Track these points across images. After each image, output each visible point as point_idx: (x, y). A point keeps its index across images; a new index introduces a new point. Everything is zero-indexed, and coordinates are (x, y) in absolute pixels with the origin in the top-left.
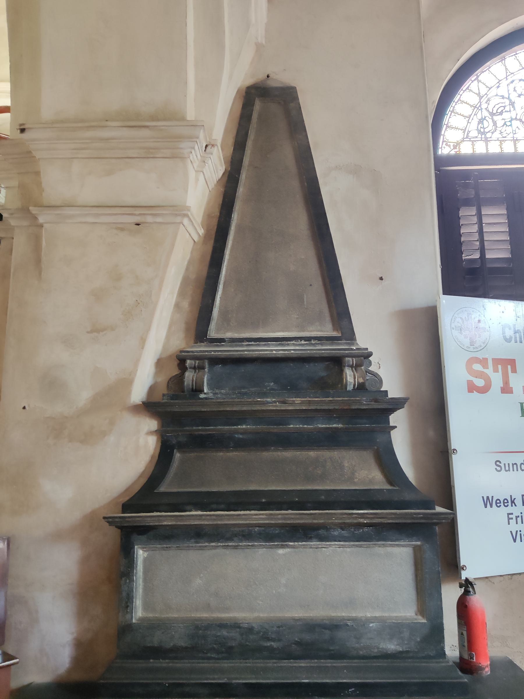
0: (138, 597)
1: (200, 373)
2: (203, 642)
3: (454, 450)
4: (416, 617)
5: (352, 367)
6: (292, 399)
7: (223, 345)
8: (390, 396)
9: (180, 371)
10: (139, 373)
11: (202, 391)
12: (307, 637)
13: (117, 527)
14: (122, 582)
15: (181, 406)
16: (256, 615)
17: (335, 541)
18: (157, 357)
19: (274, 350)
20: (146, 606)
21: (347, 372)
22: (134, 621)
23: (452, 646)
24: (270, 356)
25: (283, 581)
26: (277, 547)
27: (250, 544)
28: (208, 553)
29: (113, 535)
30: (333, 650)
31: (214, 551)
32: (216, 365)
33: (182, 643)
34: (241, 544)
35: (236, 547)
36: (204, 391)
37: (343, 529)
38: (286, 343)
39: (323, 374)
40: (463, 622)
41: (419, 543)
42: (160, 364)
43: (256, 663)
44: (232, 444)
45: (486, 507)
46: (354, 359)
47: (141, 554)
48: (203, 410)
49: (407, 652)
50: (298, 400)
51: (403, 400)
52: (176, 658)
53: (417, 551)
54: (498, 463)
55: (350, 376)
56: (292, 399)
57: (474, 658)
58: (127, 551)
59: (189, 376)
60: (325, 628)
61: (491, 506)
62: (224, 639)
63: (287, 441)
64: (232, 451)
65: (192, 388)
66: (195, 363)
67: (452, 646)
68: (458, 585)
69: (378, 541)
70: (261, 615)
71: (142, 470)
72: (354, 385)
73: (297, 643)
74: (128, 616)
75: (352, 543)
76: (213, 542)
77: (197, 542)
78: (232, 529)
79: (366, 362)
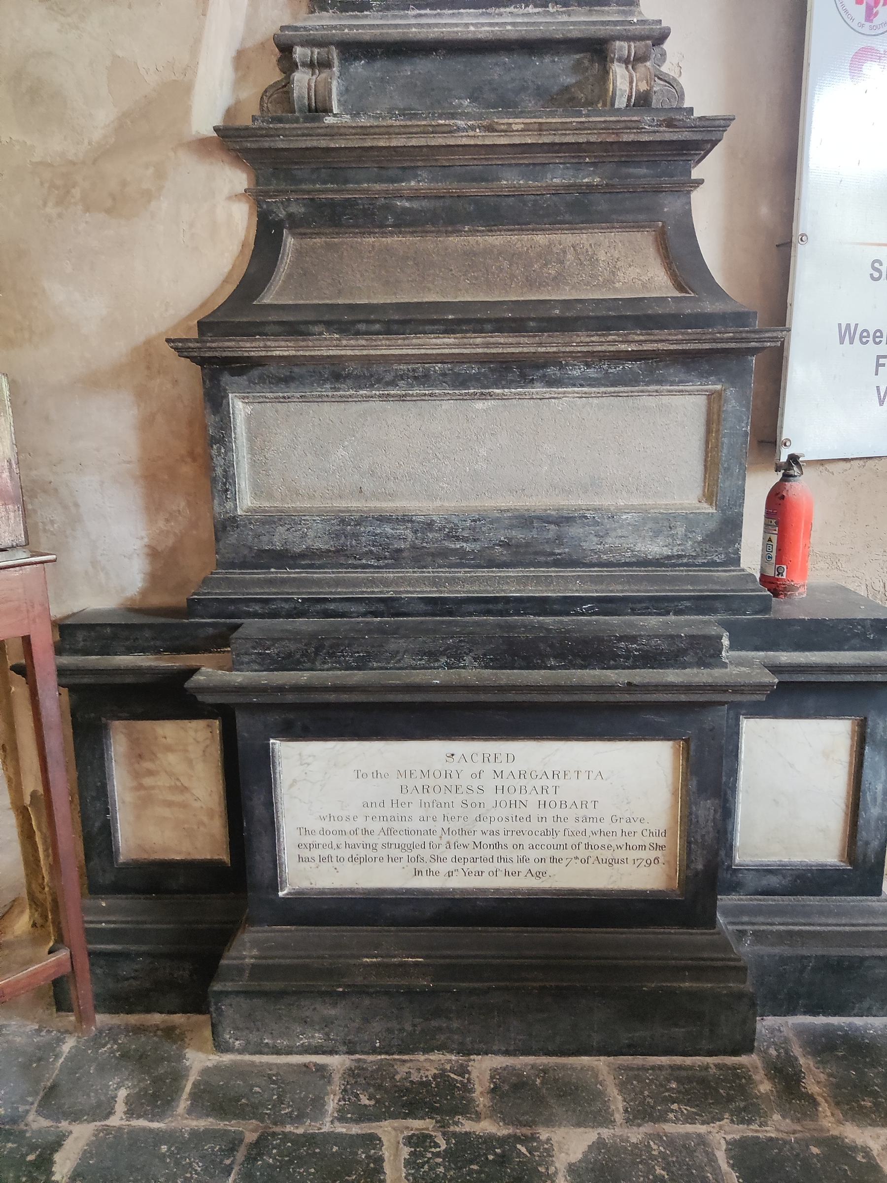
0: (228, 678)
1: (323, 75)
2: (354, 542)
3: (803, 235)
4: (699, 505)
5: (626, 62)
6: (506, 121)
7: (367, 16)
8: (696, 114)
9: (284, 75)
10: (202, 70)
11: (328, 110)
12: (519, 535)
13: (193, 359)
14: (214, 452)
15: (292, 138)
16: (438, 503)
17: (574, 385)
18: (236, 46)
19: (472, 24)
20: (258, 491)
21: (618, 71)
22: (239, 512)
23: (752, 554)
24: (464, 37)
25: (483, 452)
26: (473, 397)
27: (427, 392)
28: (355, 408)
29: (186, 376)
30: (560, 554)
31: (365, 405)
32: (354, 60)
33: (319, 545)
34: (411, 392)
35: (402, 398)
36: (331, 111)
37: (588, 365)
38: (497, 11)
39: (569, 80)
40: (774, 521)
41: (718, 387)
42: (241, 60)
43: (437, 572)
44: (391, 220)
45: (842, 342)
46: (632, 44)
47: (240, 409)
48: (333, 145)
49: (679, 557)
50: (518, 123)
51: (722, 122)
52: (311, 566)
53: (714, 399)
54: (876, 275)
55: (623, 77)
56: (506, 121)
57: (784, 574)
58: (215, 401)
59: (302, 79)
60: (549, 523)
61: (851, 342)
62: (388, 538)
63: (492, 215)
64: (392, 234)
65: (309, 105)
66: (312, 53)
67: (752, 554)
68: (774, 466)
69: (648, 384)
70: (446, 504)
71: (227, 270)
72: (630, 98)
73: (503, 544)
74: (229, 505)
75: (603, 389)
76: (361, 388)
77: (335, 389)
78: (395, 367)
79: (655, 52)
